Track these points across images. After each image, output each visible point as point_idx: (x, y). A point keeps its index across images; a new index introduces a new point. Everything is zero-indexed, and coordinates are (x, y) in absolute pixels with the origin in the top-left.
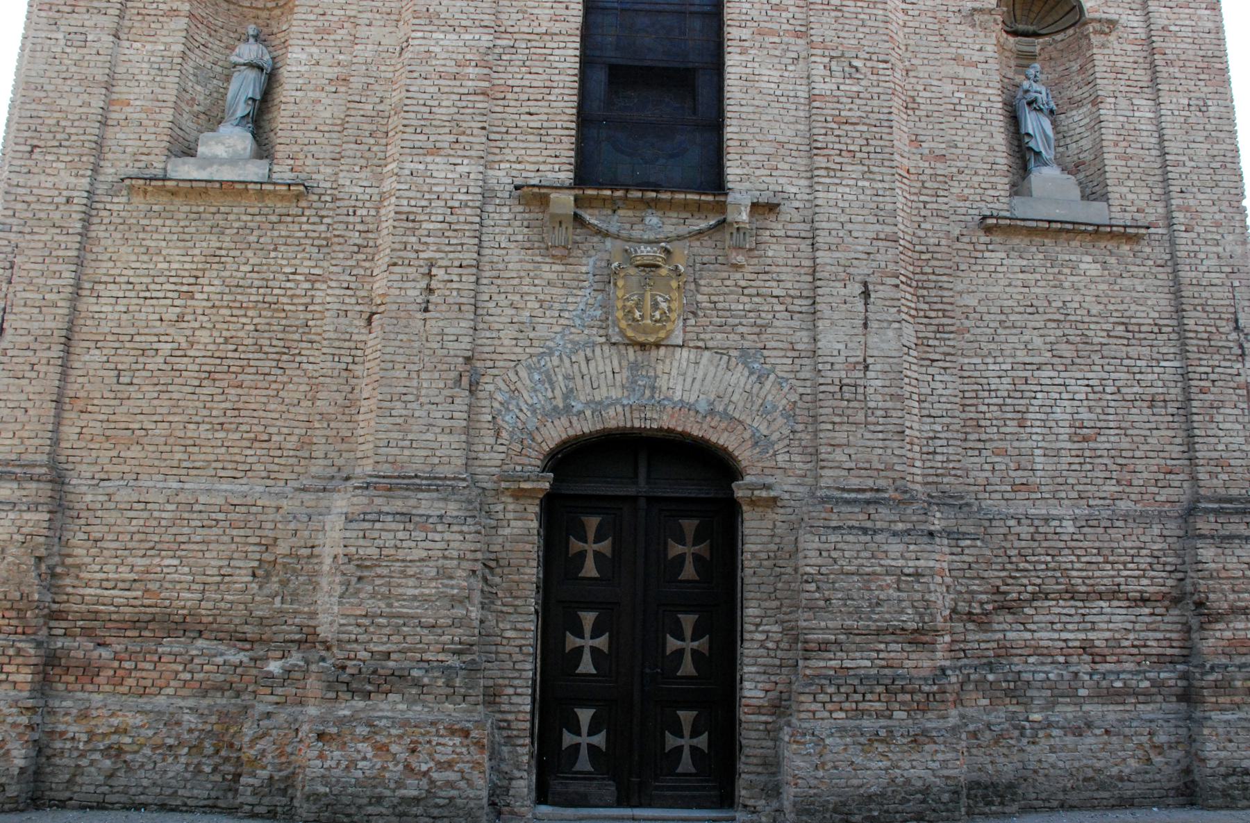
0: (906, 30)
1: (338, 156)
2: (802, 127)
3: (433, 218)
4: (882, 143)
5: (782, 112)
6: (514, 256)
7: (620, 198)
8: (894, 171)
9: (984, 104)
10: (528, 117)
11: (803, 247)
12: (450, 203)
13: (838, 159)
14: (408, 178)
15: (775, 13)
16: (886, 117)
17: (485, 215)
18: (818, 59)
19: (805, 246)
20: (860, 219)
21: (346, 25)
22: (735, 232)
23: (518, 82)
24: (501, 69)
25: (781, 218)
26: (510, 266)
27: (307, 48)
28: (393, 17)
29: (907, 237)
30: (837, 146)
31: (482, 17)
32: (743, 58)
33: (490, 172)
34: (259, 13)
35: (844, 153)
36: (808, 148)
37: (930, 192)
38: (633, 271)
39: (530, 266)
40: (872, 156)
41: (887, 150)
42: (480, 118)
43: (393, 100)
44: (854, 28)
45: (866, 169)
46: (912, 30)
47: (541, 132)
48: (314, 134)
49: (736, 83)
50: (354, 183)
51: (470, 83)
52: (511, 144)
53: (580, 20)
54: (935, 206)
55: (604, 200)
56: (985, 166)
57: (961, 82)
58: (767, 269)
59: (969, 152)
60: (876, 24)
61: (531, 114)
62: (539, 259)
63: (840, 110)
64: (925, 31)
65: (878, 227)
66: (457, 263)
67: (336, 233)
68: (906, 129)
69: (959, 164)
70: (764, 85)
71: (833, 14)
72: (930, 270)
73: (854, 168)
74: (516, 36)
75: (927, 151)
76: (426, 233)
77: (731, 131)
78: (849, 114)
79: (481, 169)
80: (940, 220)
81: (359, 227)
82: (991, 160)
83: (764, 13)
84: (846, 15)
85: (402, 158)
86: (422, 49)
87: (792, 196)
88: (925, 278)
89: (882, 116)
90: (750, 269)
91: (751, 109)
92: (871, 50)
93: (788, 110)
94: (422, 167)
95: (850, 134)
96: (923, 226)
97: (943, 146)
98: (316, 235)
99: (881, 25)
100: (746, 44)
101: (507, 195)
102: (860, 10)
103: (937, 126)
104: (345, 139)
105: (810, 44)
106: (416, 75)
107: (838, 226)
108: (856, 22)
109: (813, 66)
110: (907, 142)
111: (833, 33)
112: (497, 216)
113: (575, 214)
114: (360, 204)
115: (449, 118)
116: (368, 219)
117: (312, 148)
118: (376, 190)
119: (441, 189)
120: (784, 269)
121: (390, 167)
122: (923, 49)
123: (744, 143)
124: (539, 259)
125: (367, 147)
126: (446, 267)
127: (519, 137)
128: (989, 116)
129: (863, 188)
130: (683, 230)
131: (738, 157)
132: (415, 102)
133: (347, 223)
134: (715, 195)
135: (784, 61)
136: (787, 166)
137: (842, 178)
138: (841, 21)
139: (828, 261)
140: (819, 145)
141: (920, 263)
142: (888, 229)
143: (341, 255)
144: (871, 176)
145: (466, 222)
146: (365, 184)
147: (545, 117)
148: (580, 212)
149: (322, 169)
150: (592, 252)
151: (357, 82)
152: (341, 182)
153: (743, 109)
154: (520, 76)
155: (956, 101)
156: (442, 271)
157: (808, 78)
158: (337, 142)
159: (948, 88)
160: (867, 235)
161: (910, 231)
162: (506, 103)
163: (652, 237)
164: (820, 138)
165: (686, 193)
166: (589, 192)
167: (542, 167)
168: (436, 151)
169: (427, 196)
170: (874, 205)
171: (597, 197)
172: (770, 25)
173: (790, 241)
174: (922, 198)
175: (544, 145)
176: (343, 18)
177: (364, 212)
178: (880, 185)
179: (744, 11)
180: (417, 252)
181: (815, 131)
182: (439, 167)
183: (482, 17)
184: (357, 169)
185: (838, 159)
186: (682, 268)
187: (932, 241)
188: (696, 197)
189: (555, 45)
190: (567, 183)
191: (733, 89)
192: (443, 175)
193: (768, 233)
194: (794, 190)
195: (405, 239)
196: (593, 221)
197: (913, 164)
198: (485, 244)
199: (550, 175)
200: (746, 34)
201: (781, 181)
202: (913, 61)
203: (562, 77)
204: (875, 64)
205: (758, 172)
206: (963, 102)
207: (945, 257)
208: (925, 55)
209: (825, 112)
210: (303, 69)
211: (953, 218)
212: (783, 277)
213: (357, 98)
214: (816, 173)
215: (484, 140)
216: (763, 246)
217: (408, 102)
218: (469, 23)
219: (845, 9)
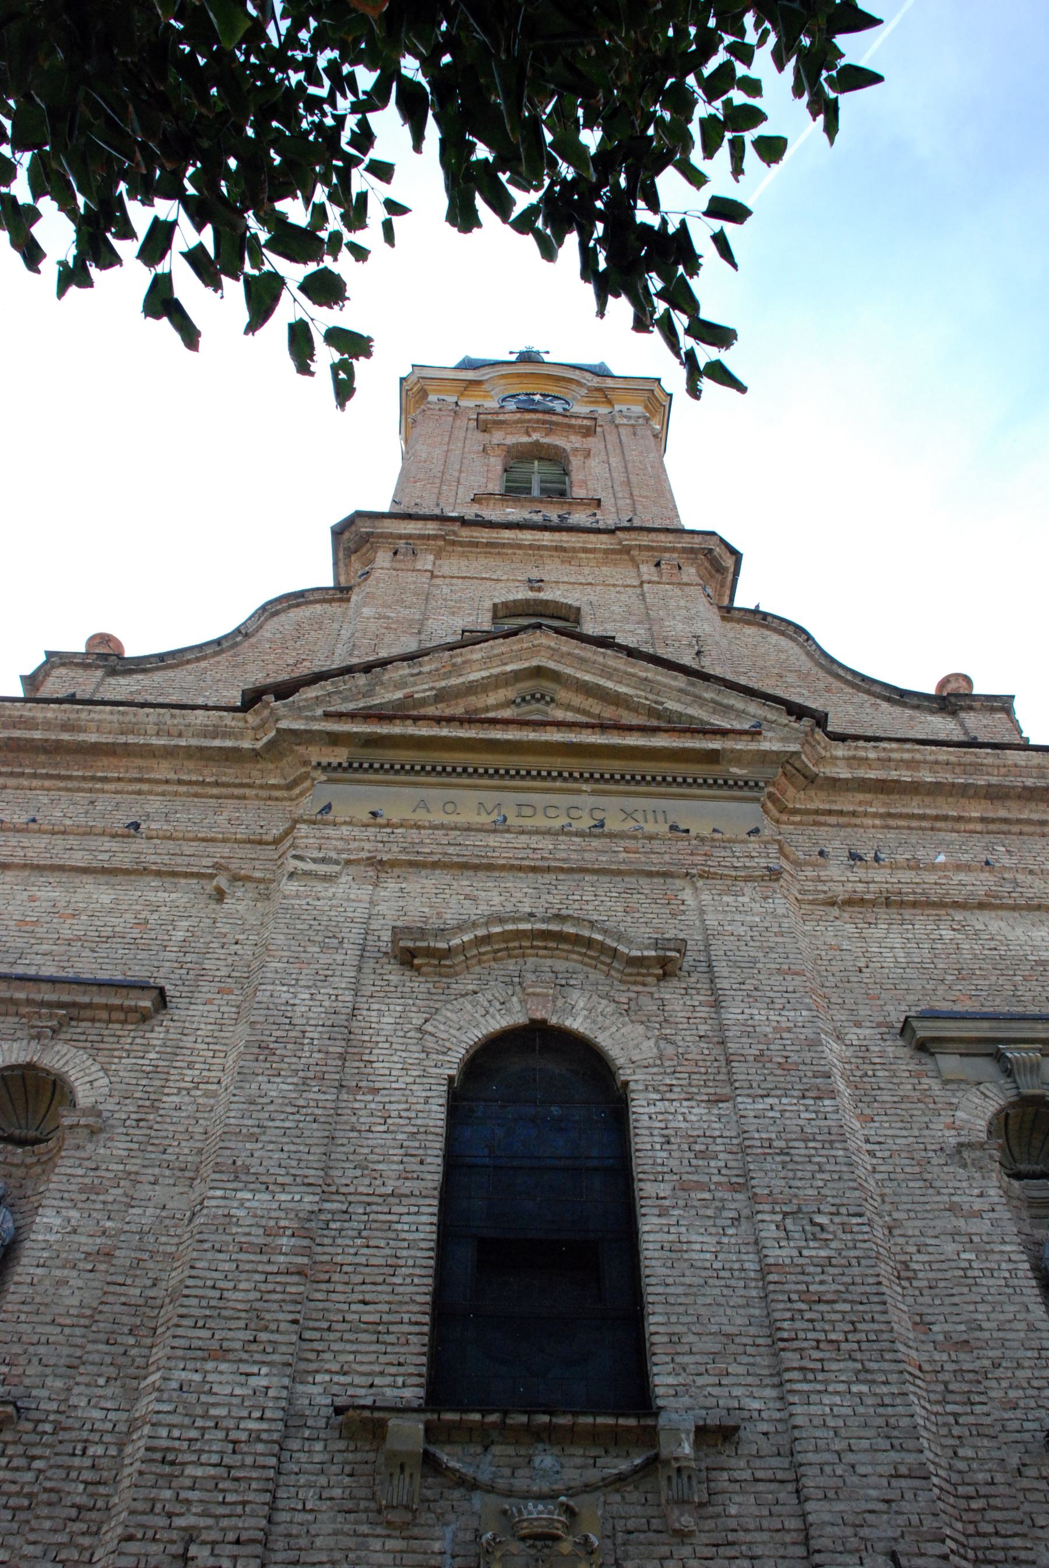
0: (878, 1176)
1: (76, 1362)
2: (757, 1312)
3: (204, 1458)
4: (875, 1326)
5: (725, 1291)
6: (326, 1524)
7: (493, 1424)
8: (902, 1366)
9: (1004, 1266)
10: (361, 1307)
11: (782, 1496)
12: (234, 1435)
13: (816, 1355)
14: (175, 1394)
15: (700, 1162)
16: (874, 1289)
17: (285, 1455)
18: (767, 1217)
19: (785, 1493)
20: (865, 1444)
21: (122, 1183)
22: (674, 1474)
23: (350, 1259)
24: (326, 1241)
25: (743, 1450)
26: (319, 1542)
27: (64, 1212)
28: (187, 1174)
29: (942, 1473)
30: (810, 1335)
31: (307, 1172)
32: (664, 1221)
33: (300, 1388)
34: (14, 1170)
35: (822, 1345)
36: (769, 1341)
37: (957, 1398)
38: (515, 1547)
39: (350, 1542)
40: (864, 1346)
41: (885, 1336)
42: (291, 1308)
43: (172, 1283)
44: (809, 1175)
45: (859, 1366)
46: (885, 1176)
47: (378, 1329)
48: (49, 1329)
49: (656, 1254)
50: (93, 1407)
51: (282, 1259)
52: (335, 1347)
53: (438, 1177)
54: (971, 1419)
55: (471, 1430)
56: (1029, 1354)
57: (966, 1239)
58: (731, 1537)
59: (1001, 1334)
60: (837, 1168)
61: (365, 1303)
62: (365, 1529)
63: (807, 1284)
64: (902, 1176)
65: (894, 1456)
66: (231, 1536)
67: (48, 1484)
68: (905, 1308)
69: (991, 1354)
70: (695, 1256)
71: (778, 1159)
72: (990, 1529)
73: (842, 1365)
74: (350, 1198)
75: (940, 1338)
76: (188, 1483)
77: (655, 1322)
78: (822, 1288)
79: (286, 1381)
80: (986, 1442)
81: (87, 1475)
82: (1036, 1344)
83: (685, 1162)
84: (796, 1159)
85: (172, 1364)
86: (220, 1212)
87: (755, 1414)
88: (984, 1542)
89: (868, 1289)
90: (704, 1538)
91: (680, 1290)
92: (837, 1201)
93: (734, 1288)
94: (197, 1377)
95: (827, 1317)
96: (961, 1452)
97: (963, 1327)
98: (14, 1488)
99: (845, 1168)
100: (667, 1203)
101: (322, 1423)
102: (813, 1152)
103: (947, 1300)
104: (92, 1337)
105: (754, 1198)
106: (207, 1246)
107: (832, 1458)
108: (809, 1167)
109: (761, 1226)
110: (910, 1326)
111: (783, 1183)
112: (303, 1457)
113: (426, 1452)
114: (96, 1437)
115: (247, 1306)
116: (104, 1462)
117: (42, 1350)
118: (124, 1416)
119: (222, 1412)
120: (758, 1536)
121: (151, 1379)
122: (904, 1199)
123: (675, 1339)
124: (365, 1529)
125: (122, 1350)
126: (214, 1543)
127: (347, 1336)
128: (1016, 1282)
129: (860, 1395)
130: (593, 1475)
131: (668, 1359)
132: (200, 1283)
133: (69, 1468)
134: (638, 1417)
135: (720, 1222)
136: (742, 1370)
137: (826, 1382)
138: (790, 1167)
139: (827, 1517)
140: (785, 1335)
141: (970, 1516)
142: (911, 1458)
143: (47, 1524)
144: (869, 1377)
145: (254, 1466)
146: (109, 1405)
147: (385, 1308)
148: (432, 1449)
149: (49, 1382)
150: (451, 1517)
151: (123, 1257)
152: (74, 1401)
153: (669, 1290)
154: (352, 1251)
155: (965, 1265)
156: (206, 1551)
157: (756, 1243)
158: (79, 1341)
159: (950, 1248)
160: (880, 1469)
161: (944, 1462)
162: (330, 1287)
163: (545, 1488)
164: (786, 1325)
165: (595, 1415)
166: (448, 1416)
167: (378, 1381)
168: (222, 1353)
169: (199, 1423)
170: (881, 1421)
171: (458, 1425)
172: (695, 1178)
173: (761, 1487)
174: (950, 1408)
175: (382, 1348)
176: (120, 1174)
177: (99, 1450)
178: (885, 1389)
179: (659, 1161)
180: (170, 1515)
181: (777, 1315)
182: (224, 1380)
183: (307, 1172)
184: (101, 1381)
185: (816, 1355)
186: (595, 1540)
187: (980, 1477)
188: (611, 1421)
189: (405, 1210)
190: (415, 1404)
191: (654, 1263)
192: (227, 1390)
193: (725, 1475)
194: (756, 1405)
195: (154, 1493)
196: (453, 1464)
197: (925, 1357)
198: (281, 1504)
199: (388, 1392)
200: (664, 1189)
201: (737, 1392)
202: (896, 1215)
203: (412, 1252)
204: (845, 1219)
205: (700, 1381)
206: (975, 1265)
207: (1008, 1503)
208: (909, 1206)
209: (787, 1287)
210: (52, 1238)
211: (1003, 1437)
212: (758, 1551)
213: (120, 1279)
214: (787, 1376)
215: (294, 1338)
216: (719, 1498)
217: (190, 1282)
218: (288, 1180)
219: (793, 1151)
